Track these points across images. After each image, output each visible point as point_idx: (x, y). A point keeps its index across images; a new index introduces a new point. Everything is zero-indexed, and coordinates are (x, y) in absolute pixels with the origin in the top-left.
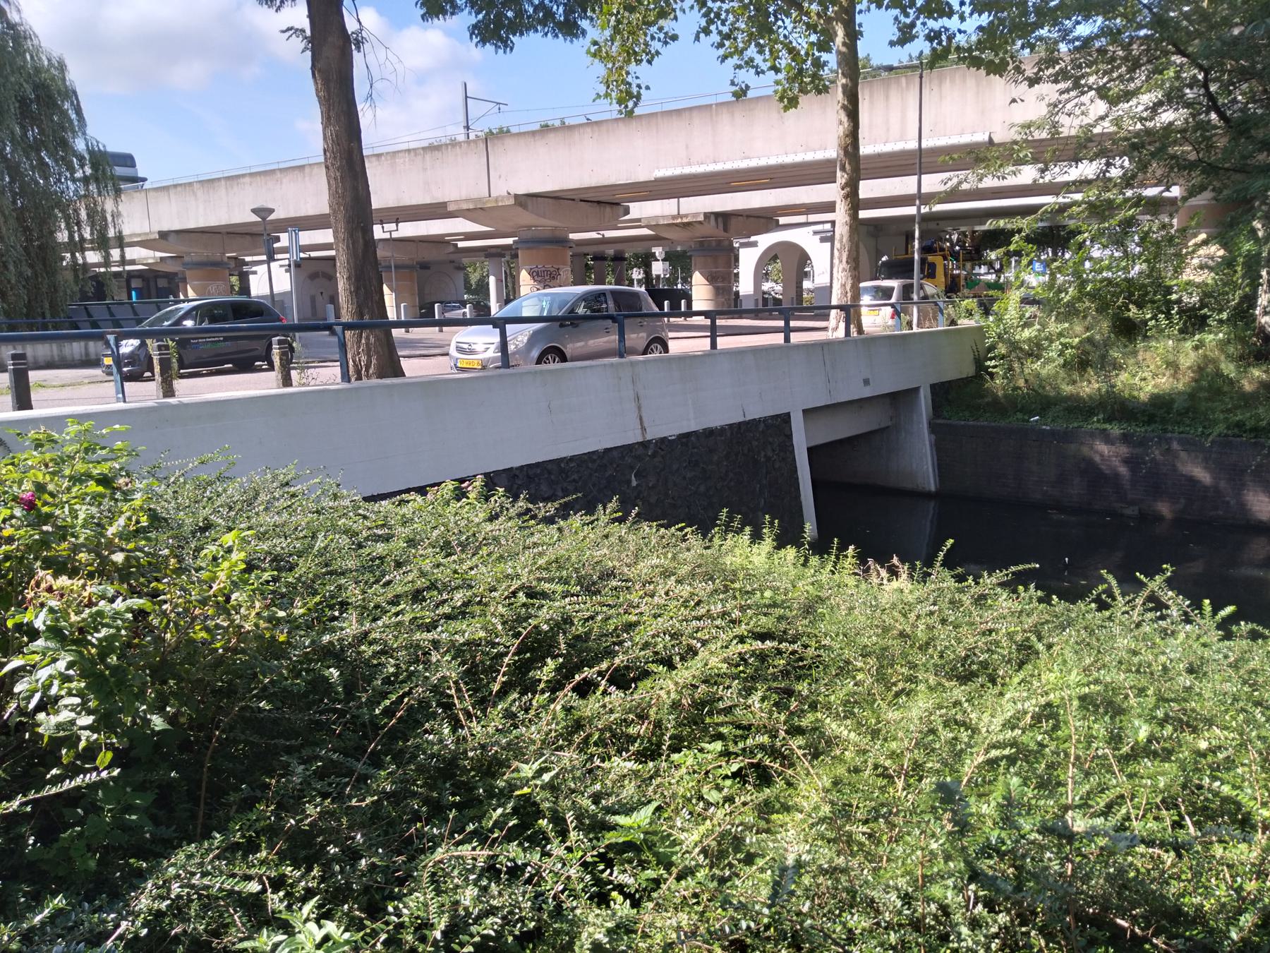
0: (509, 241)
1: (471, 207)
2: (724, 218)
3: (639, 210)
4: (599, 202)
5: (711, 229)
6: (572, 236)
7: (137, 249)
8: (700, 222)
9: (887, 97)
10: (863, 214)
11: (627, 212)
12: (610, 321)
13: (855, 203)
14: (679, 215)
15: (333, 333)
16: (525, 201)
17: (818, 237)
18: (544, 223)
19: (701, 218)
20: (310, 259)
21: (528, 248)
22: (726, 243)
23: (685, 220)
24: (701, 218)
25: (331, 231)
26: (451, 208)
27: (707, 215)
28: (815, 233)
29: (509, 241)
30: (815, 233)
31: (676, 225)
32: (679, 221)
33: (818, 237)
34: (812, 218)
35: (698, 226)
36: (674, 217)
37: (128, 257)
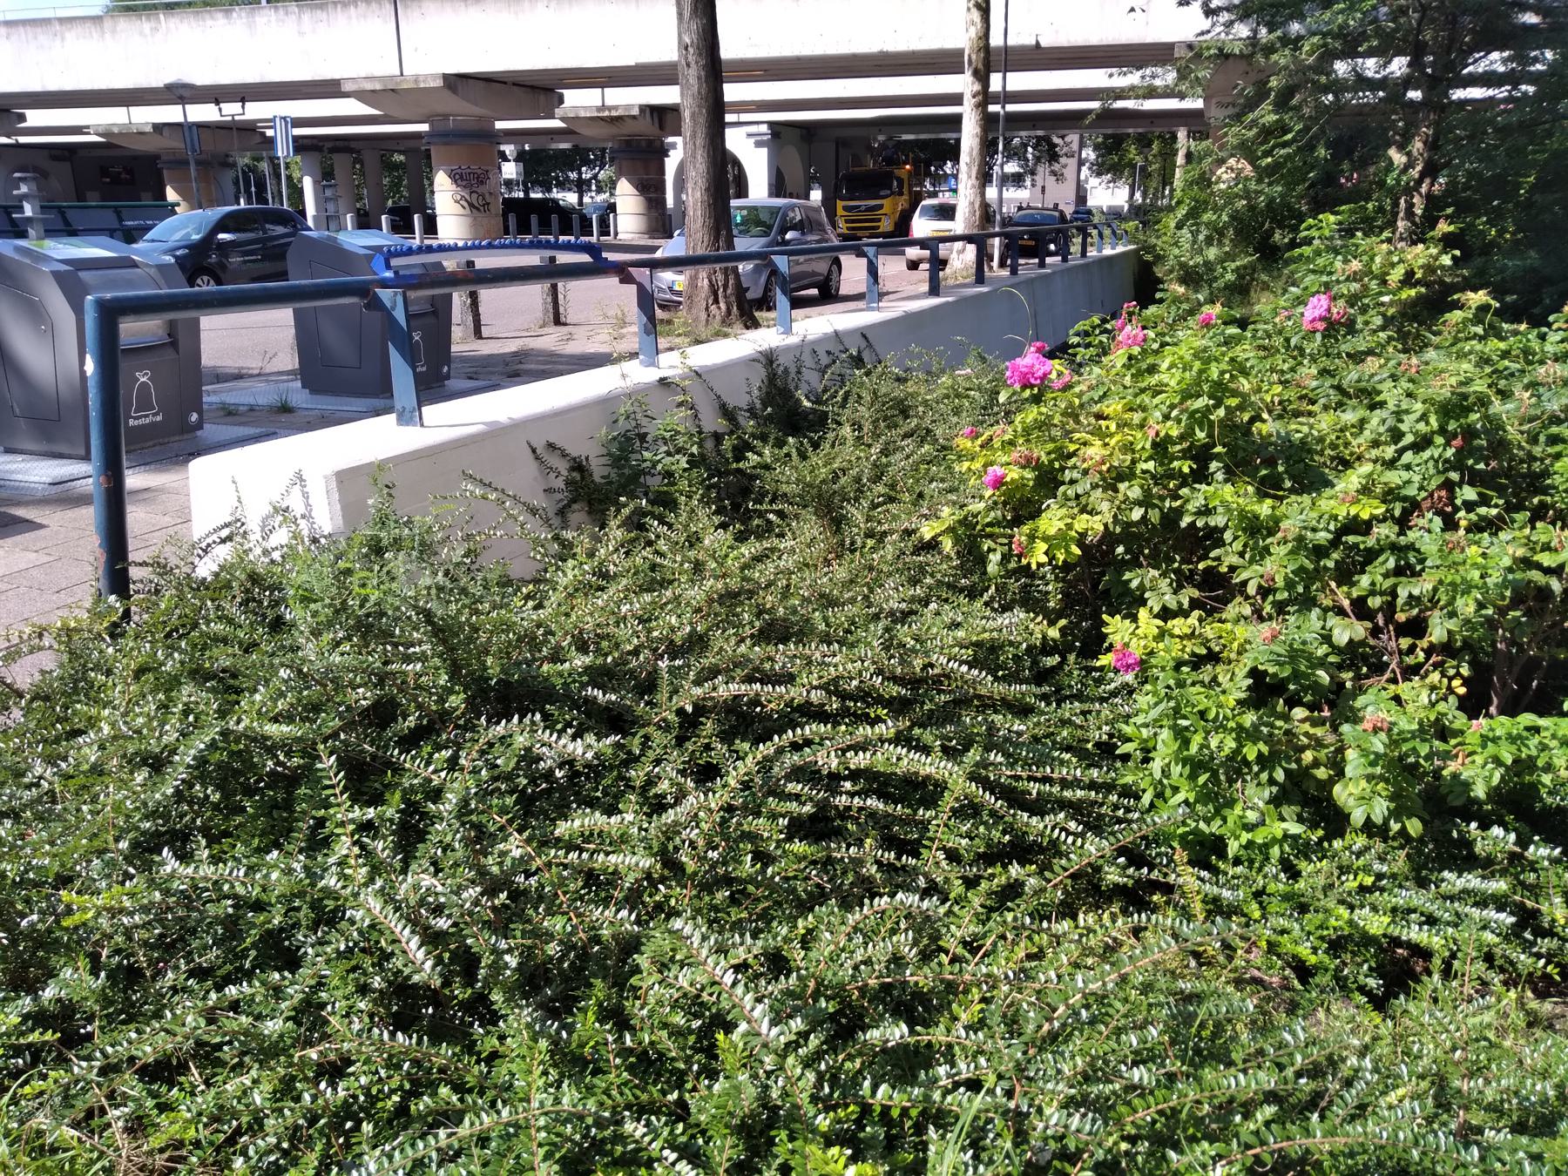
0: (424, 127)
1: (378, 87)
2: (1182, 96)
3: (35, 118)
4: (533, 87)
5: (647, 127)
6: (500, 125)
7: (352, 101)
8: (634, 117)
9: (63, 39)
10: (993, 108)
11: (561, 101)
12: (614, 281)
13: (985, 97)
14: (603, 107)
15: (627, 279)
16: (455, 82)
17: (752, 140)
18: (463, 109)
19: (636, 112)
20: (18, 146)
21: (446, 144)
22: (657, 144)
23: (614, 113)
24: (636, 112)
25: (677, 88)
26: (347, 87)
27: (643, 108)
28: (750, 135)
29: (424, 127)
30: (750, 135)
31: (602, 119)
32: (606, 113)
33: (752, 140)
34: (745, 117)
35: (630, 121)
36: (599, 109)
37: (608, 102)
